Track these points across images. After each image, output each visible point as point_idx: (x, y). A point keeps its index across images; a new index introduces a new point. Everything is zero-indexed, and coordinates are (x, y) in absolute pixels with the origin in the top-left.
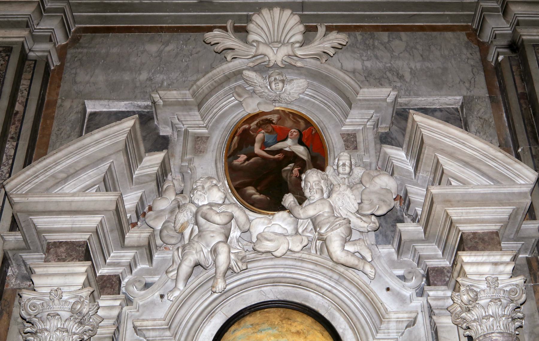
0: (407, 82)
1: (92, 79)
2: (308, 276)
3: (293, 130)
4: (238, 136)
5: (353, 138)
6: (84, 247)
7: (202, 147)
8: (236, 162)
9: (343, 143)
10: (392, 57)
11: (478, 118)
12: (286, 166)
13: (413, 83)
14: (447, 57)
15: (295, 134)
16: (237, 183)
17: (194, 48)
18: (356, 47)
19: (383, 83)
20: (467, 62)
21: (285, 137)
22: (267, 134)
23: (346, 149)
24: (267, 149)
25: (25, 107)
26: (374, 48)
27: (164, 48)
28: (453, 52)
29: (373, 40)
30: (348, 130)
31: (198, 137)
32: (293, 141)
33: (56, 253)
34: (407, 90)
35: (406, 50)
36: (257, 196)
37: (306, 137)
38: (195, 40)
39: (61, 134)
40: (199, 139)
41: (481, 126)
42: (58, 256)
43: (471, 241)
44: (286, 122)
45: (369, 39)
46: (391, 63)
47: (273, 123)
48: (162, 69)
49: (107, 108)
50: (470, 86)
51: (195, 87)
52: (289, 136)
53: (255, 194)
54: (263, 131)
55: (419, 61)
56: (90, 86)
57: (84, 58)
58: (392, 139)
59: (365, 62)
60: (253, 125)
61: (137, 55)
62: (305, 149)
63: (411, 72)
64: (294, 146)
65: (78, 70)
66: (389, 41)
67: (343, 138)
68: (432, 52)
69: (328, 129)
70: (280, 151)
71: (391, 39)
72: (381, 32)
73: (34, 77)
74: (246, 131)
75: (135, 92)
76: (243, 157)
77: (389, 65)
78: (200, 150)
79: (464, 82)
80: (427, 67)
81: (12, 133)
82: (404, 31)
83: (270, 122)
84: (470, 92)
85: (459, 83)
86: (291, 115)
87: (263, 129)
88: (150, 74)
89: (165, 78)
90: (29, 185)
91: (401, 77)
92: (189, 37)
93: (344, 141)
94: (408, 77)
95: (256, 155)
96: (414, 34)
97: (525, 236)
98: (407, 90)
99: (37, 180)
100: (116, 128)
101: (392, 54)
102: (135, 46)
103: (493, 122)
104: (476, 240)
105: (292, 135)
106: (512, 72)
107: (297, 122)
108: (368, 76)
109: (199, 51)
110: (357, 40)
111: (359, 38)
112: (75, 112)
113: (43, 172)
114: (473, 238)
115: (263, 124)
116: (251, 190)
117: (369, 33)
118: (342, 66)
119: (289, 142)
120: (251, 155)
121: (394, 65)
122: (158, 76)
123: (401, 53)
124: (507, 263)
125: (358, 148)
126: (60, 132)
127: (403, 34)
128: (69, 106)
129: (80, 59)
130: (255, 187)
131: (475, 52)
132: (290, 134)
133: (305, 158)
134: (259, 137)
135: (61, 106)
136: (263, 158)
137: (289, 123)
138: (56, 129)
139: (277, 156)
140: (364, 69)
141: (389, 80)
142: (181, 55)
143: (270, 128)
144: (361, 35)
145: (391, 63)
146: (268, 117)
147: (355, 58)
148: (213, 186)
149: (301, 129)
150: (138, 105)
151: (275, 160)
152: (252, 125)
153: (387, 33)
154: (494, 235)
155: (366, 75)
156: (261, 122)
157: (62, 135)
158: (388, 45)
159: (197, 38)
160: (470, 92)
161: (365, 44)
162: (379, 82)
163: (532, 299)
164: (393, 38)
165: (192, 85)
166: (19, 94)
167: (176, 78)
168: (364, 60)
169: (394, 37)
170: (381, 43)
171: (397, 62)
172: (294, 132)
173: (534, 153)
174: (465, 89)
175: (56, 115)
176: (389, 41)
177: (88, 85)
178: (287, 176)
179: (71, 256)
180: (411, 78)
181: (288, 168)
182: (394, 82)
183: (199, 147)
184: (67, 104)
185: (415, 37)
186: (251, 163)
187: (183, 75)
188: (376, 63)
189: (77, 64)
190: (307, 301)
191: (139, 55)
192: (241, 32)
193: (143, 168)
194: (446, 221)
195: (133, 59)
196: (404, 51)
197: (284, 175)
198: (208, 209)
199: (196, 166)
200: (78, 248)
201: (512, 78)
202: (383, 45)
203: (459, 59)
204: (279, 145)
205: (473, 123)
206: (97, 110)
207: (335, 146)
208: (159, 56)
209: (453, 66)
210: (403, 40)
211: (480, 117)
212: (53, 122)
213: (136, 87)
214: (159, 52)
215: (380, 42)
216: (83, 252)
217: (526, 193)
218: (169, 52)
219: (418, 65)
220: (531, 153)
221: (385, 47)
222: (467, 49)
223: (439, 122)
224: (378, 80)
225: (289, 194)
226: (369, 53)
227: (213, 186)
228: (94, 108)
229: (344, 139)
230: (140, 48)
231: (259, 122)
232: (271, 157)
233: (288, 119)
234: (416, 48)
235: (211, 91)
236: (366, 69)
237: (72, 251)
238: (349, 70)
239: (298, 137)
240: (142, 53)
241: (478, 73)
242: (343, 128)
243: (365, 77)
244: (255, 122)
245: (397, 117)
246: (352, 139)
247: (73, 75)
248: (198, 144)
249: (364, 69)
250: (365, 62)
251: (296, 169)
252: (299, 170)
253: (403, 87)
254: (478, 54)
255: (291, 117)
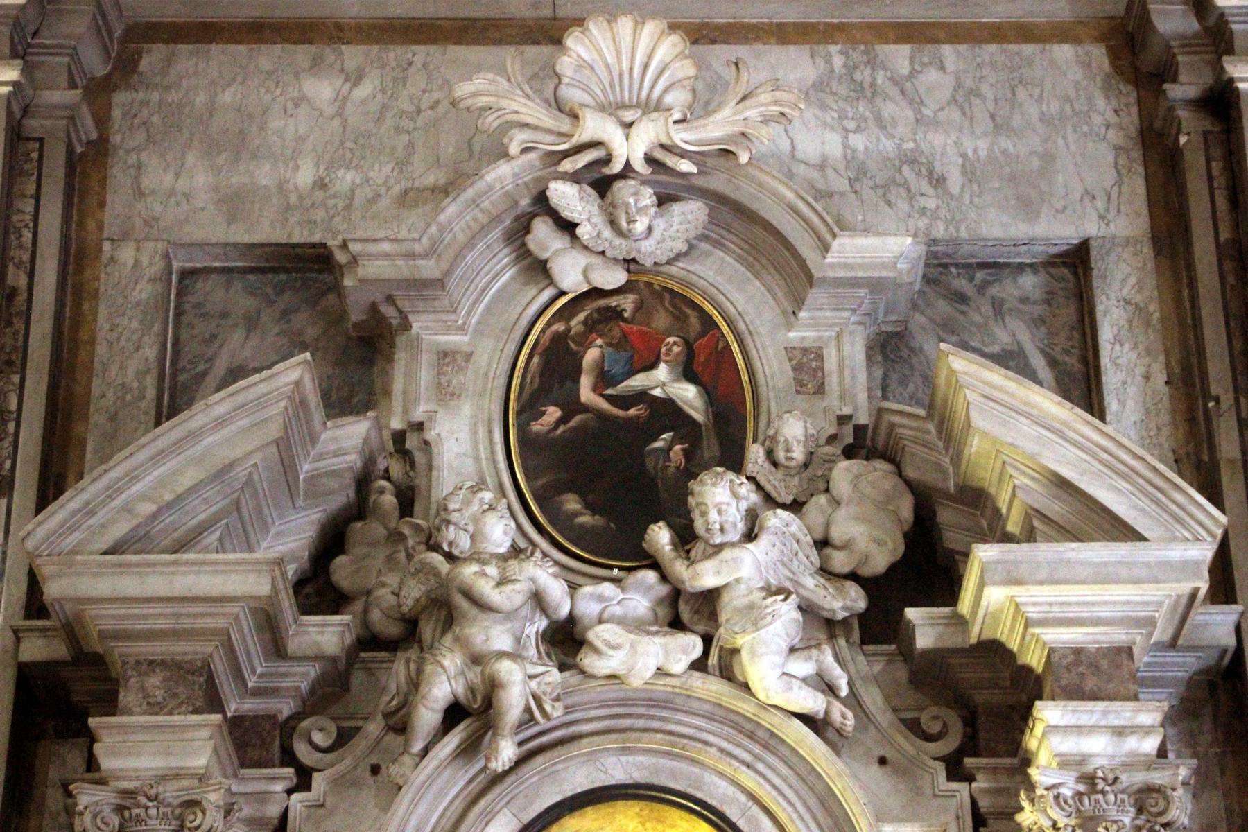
0: (952, 196)
1: (181, 182)
2: (701, 729)
3: (671, 340)
4: (541, 354)
5: (815, 359)
6: (201, 675)
7: (454, 382)
8: (536, 427)
9: (790, 373)
10: (917, 121)
11: (1122, 303)
12: (655, 439)
13: (967, 200)
14: (1056, 122)
15: (676, 349)
16: (540, 483)
17: (424, 91)
18: (828, 90)
19: (892, 198)
20: (1105, 138)
21: (653, 359)
22: (610, 349)
23: (798, 392)
24: (610, 391)
25: (31, 275)
26: (874, 94)
27: (351, 90)
28: (1072, 106)
29: (873, 69)
30: (803, 339)
31: (446, 354)
32: (671, 371)
33: (142, 688)
34: (953, 218)
35: (953, 100)
36: (585, 519)
37: (702, 359)
38: (425, 65)
39: (118, 339)
40: (447, 360)
41: (1127, 326)
42: (146, 696)
43: (1069, 671)
44: (656, 316)
45: (862, 67)
46: (915, 141)
47: (625, 320)
48: (348, 155)
49: (222, 261)
50: (1107, 210)
51: (434, 228)
52: (663, 357)
53: (582, 514)
54: (599, 342)
55: (985, 134)
56: (178, 204)
57: (155, 119)
58: (912, 350)
59: (851, 135)
60: (577, 322)
61: (285, 112)
62: (699, 392)
63: (963, 166)
64: (675, 385)
65: (144, 157)
66: (913, 73)
67: (790, 360)
68: (1021, 105)
69: (756, 338)
70: (642, 396)
71: (917, 67)
72: (893, 47)
73: (43, 190)
74: (560, 340)
75: (286, 220)
76: (553, 413)
77: (911, 145)
78: (450, 390)
79: (1094, 198)
80: (1005, 152)
81: (8, 350)
82: (950, 42)
83: (617, 314)
84: (1107, 225)
85: (1082, 199)
86: (667, 296)
87: (600, 336)
88: (322, 168)
89: (358, 181)
90: (76, 534)
91: (938, 182)
92: (410, 56)
93: (794, 369)
94: (955, 181)
95: (585, 409)
96: (977, 49)
97: (1202, 643)
98: (953, 218)
99: (91, 522)
100: (262, 388)
101: (920, 111)
102: (278, 83)
103: (1157, 314)
104: (1080, 669)
105: (669, 351)
106: (1210, 179)
107: (680, 318)
108: (857, 179)
109: (438, 102)
110: (832, 71)
111: (838, 61)
112: (146, 278)
113: (103, 501)
114: (1076, 663)
115: (600, 321)
116: (572, 503)
117: (862, 47)
118: (793, 148)
119: (662, 372)
120: (572, 407)
121: (922, 145)
122: (340, 173)
123: (942, 109)
124: (1146, 730)
125: (827, 388)
126: (115, 335)
127: (947, 50)
128: (130, 262)
129: (144, 123)
130: (583, 495)
131: (1127, 105)
132: (663, 350)
133: (698, 417)
134: (591, 356)
135: (112, 259)
136: (600, 415)
137: (661, 320)
138: (107, 327)
139: (632, 412)
140: (849, 157)
141: (909, 191)
142: (393, 112)
143: (617, 333)
144: (842, 52)
145: (915, 141)
146: (613, 302)
147: (825, 124)
148: (484, 511)
149: (692, 336)
150: (297, 255)
151: (629, 420)
152: (573, 323)
153: (905, 49)
154: (1124, 655)
155: (852, 175)
156: (595, 315)
157: (123, 343)
158: (908, 84)
159: (429, 59)
160: (1107, 225)
161: (853, 80)
162: (884, 195)
163: (1216, 788)
164: (924, 65)
165: (428, 226)
166: (12, 237)
167: (386, 182)
168: (846, 131)
169: (926, 60)
170: (891, 79)
171: (930, 137)
172: (675, 343)
173: (1244, 414)
174: (1094, 217)
175: (102, 288)
176: (913, 73)
177: (172, 200)
178: (655, 468)
179: (176, 695)
180: (963, 186)
181: (658, 444)
182: (922, 195)
183: (449, 382)
184: (127, 254)
185: (979, 60)
186: (574, 428)
187: (402, 172)
188: (878, 140)
189: (140, 137)
190: (699, 789)
191: (289, 113)
192: (538, 43)
193: (320, 457)
194: (1014, 618)
195: (276, 123)
196: (949, 103)
197: (650, 462)
198: (475, 573)
199: (443, 434)
200: (189, 677)
201: (1207, 198)
202: (896, 83)
203: (1085, 128)
204: (638, 381)
205: (1108, 317)
206: (198, 265)
207: (770, 384)
208: (339, 114)
209: (1068, 148)
210: (949, 70)
211: (1125, 300)
212: (97, 305)
213: (288, 207)
214: (337, 104)
215: (889, 74)
216: (200, 687)
217: (1197, 563)
218: (364, 102)
219: (983, 145)
220: (1238, 413)
221: (903, 92)
222: (1107, 97)
223: (1006, 377)
224: (880, 191)
225: (661, 524)
226: (861, 109)
227: (484, 511)
228: (190, 260)
229: (794, 362)
230: (291, 89)
231: (591, 314)
232: (620, 413)
233: (659, 306)
234: (979, 95)
235: (474, 237)
236: (853, 158)
237: (177, 683)
238: (812, 162)
239: (682, 358)
240: (297, 106)
241: (1129, 171)
242: (791, 335)
243: (850, 180)
244: (581, 316)
245: (927, 289)
246: (814, 364)
247: (133, 171)
248: (444, 374)
249: (849, 157)
250: (851, 135)
251: (678, 447)
252: (683, 450)
253: (943, 213)
254: (1134, 110)
255: (667, 304)
